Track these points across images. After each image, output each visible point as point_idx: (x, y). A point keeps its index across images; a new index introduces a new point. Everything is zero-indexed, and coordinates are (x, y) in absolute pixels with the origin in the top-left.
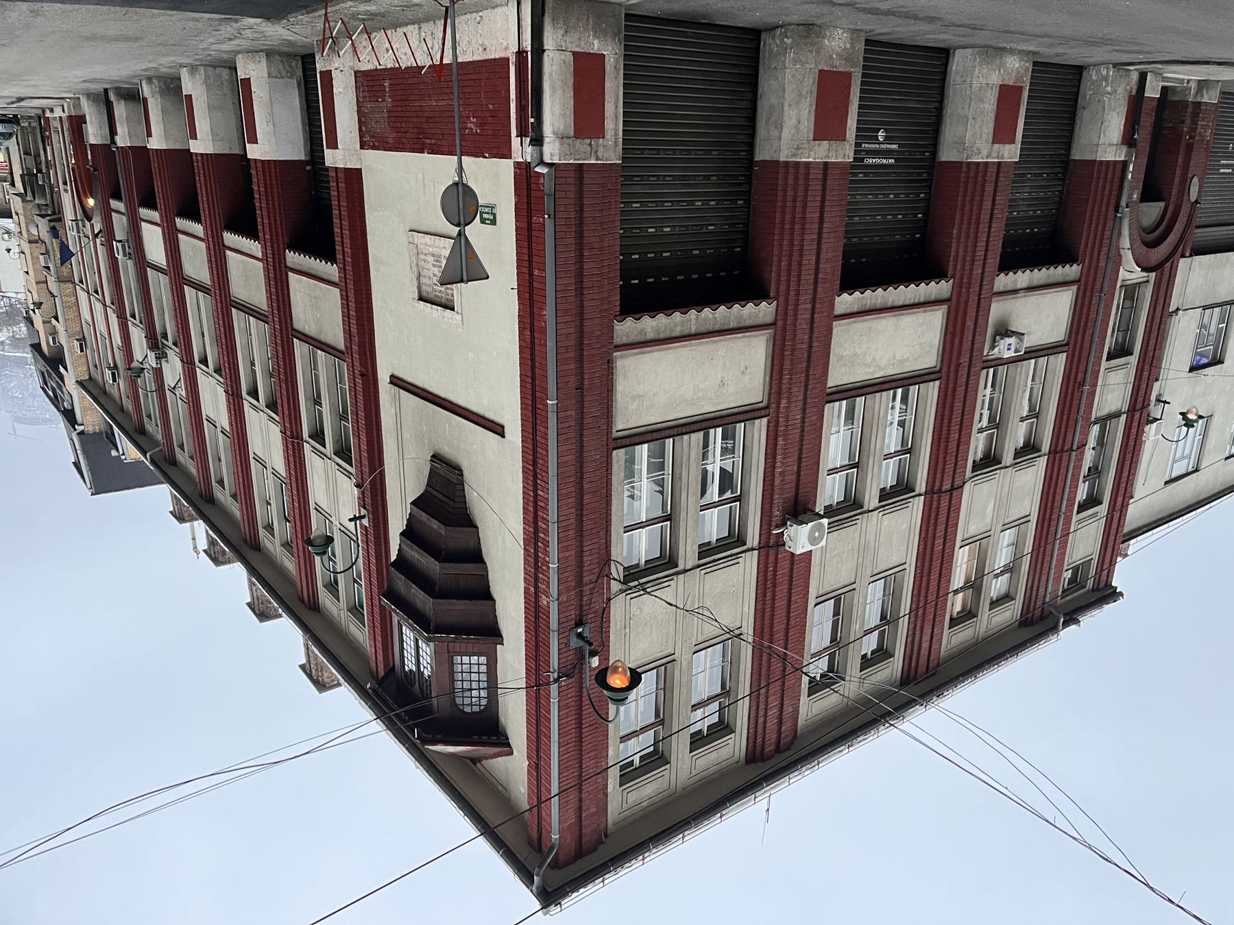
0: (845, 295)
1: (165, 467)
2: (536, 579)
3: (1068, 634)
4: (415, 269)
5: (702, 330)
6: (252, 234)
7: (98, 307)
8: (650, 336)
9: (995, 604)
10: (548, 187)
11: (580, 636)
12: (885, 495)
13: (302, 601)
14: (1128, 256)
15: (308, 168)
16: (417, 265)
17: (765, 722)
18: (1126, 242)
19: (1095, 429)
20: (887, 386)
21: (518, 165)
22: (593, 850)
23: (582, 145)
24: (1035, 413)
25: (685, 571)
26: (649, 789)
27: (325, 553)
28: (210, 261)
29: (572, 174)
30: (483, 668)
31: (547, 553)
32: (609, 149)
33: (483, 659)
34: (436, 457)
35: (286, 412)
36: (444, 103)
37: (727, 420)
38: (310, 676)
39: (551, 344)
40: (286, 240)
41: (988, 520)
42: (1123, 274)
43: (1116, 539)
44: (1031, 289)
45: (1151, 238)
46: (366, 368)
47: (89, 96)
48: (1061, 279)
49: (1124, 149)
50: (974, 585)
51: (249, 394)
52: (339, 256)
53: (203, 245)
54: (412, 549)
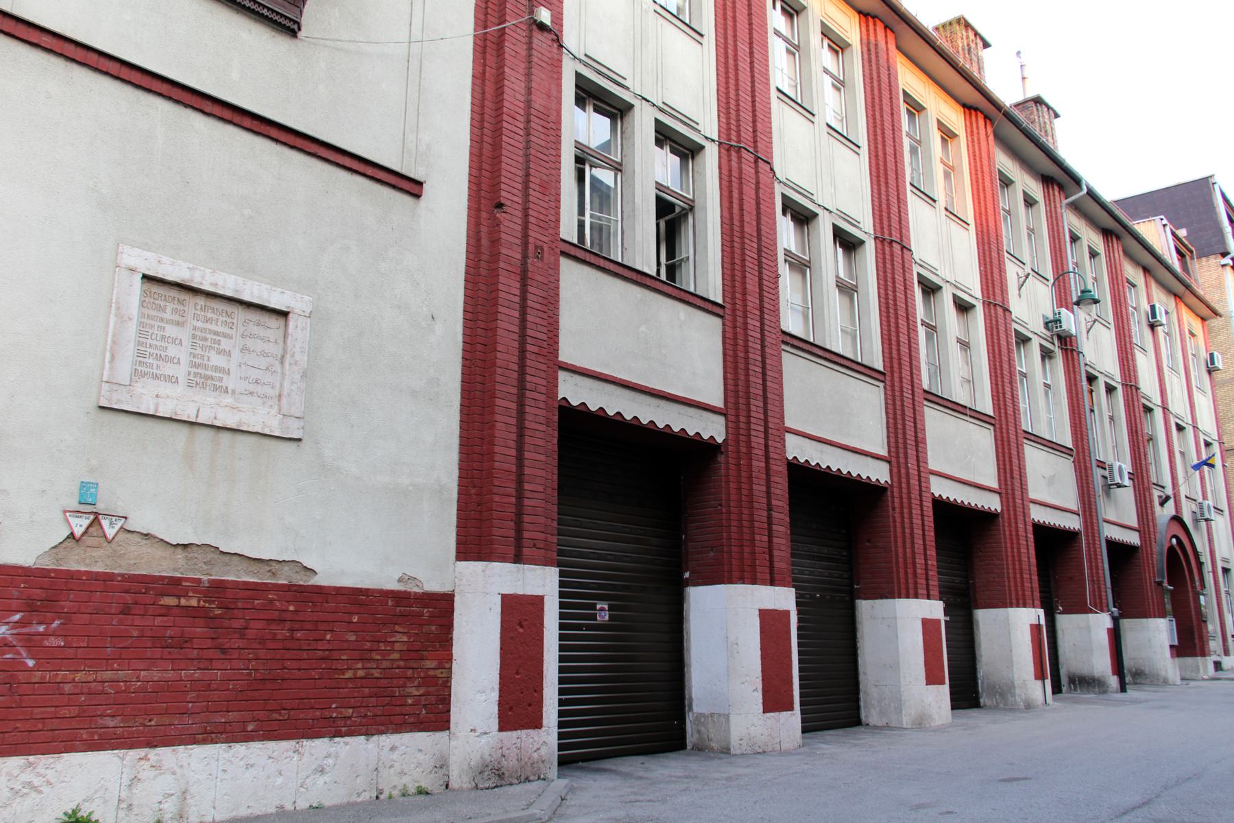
1: (1113, 226)
6: (1113, 545)
7: (1178, 405)
13: (986, 117)
35: (1002, 335)
40: (721, 458)
46: (492, 217)
51: (1114, 388)
52: (1030, 529)
53: (789, 423)
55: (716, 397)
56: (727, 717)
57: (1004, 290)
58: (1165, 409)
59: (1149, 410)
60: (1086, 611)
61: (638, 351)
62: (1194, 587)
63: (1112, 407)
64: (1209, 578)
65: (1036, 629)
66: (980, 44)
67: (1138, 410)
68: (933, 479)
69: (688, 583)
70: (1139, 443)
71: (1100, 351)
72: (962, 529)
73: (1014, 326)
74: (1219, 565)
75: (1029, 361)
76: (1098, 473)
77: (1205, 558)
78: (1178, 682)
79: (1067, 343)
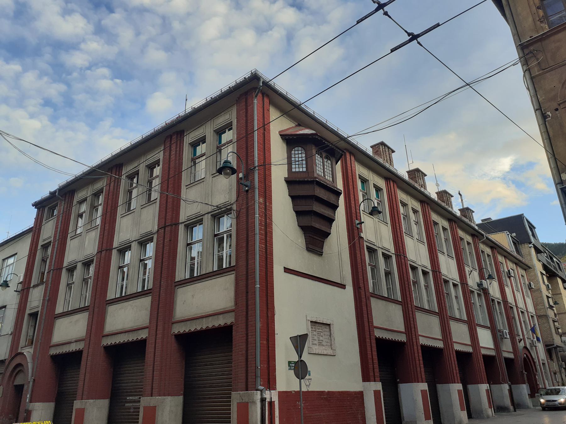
0: (144, 337)
2: (266, 209)
3: (54, 187)
4: (332, 338)
5: (201, 319)
6: (506, 359)
7: (521, 305)
8: (221, 316)
9: (85, 200)
10: (259, 380)
11: (247, 186)
12: (129, 248)
13: (393, 181)
14: (29, 359)
15: (398, 380)
16: (331, 340)
17: (176, 148)
18: (30, 366)
19: (44, 280)
20: (128, 297)
21: (275, 389)
22: (241, 95)
23: (246, 400)
24: (69, 286)
25: (208, 213)
26: (221, 121)
27: (373, 208)
28: (450, 333)
29: (249, 386)
30: (293, 166)
31: (260, 220)
32: (236, 397)
33: (293, 170)
34: (320, 254)
36: (316, 414)
37: (193, 280)
38: (389, 148)
39: (258, 312)
41: (87, 237)
42: (32, 351)
43: (35, 231)
44: (69, 343)
45: (19, 368)
47: (528, 408)
48: (57, 347)
49: (30, 409)
50: (94, 208)
54: (328, 214)
55: (402, 329)
56: (416, 422)
57: (466, 278)
58: (527, 311)
59: (512, 308)
60: (501, 383)
61: (388, 319)
62: (533, 372)
63: (500, 309)
64: (538, 367)
65: (487, 391)
66: (390, 152)
67: (508, 308)
68: (455, 344)
69: (399, 383)
70: (510, 320)
71: (494, 290)
72: (432, 356)
73: (443, 277)
74: (541, 362)
75: (476, 300)
76: (499, 334)
77: (536, 360)
78: (532, 407)
79: (485, 292)
